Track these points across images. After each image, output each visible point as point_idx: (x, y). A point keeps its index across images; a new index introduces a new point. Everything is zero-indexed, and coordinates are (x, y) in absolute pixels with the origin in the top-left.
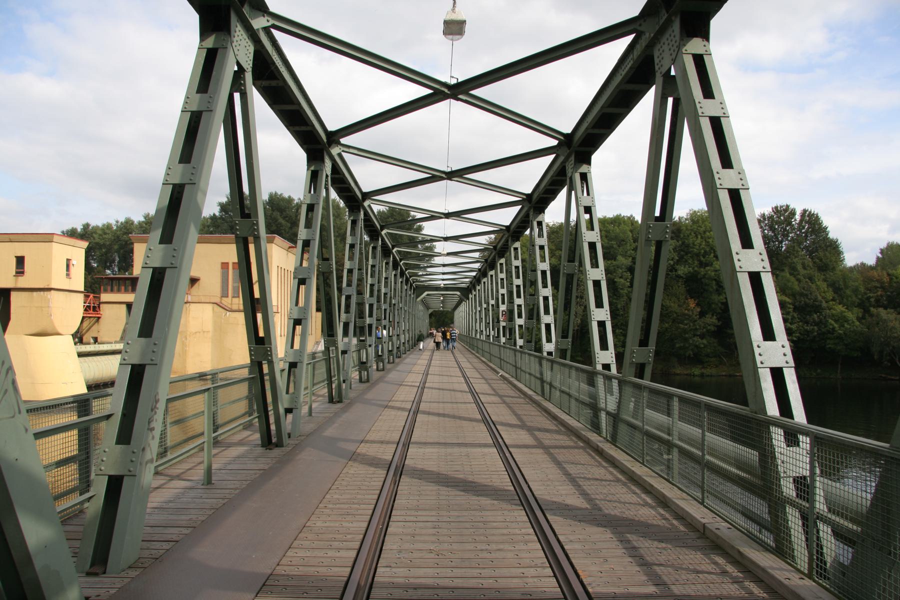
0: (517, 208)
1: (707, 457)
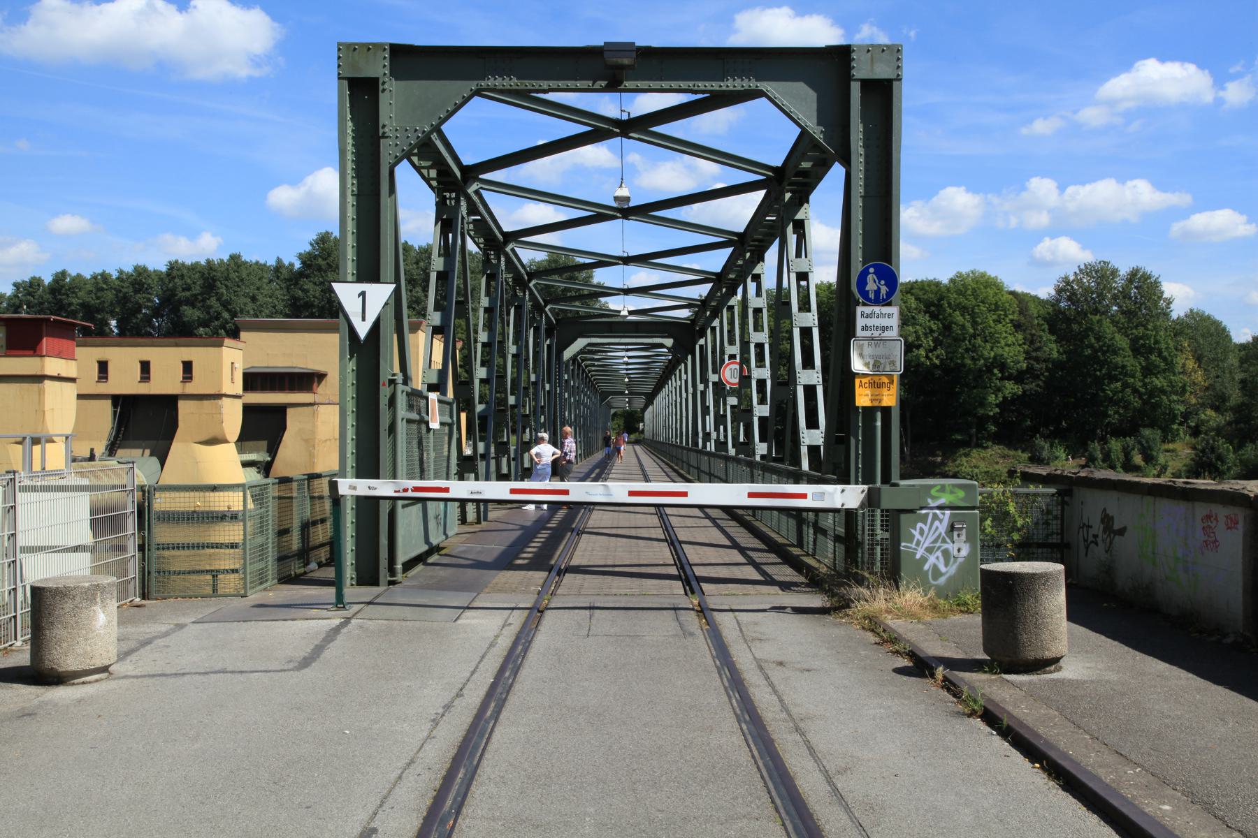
0: (760, 195)
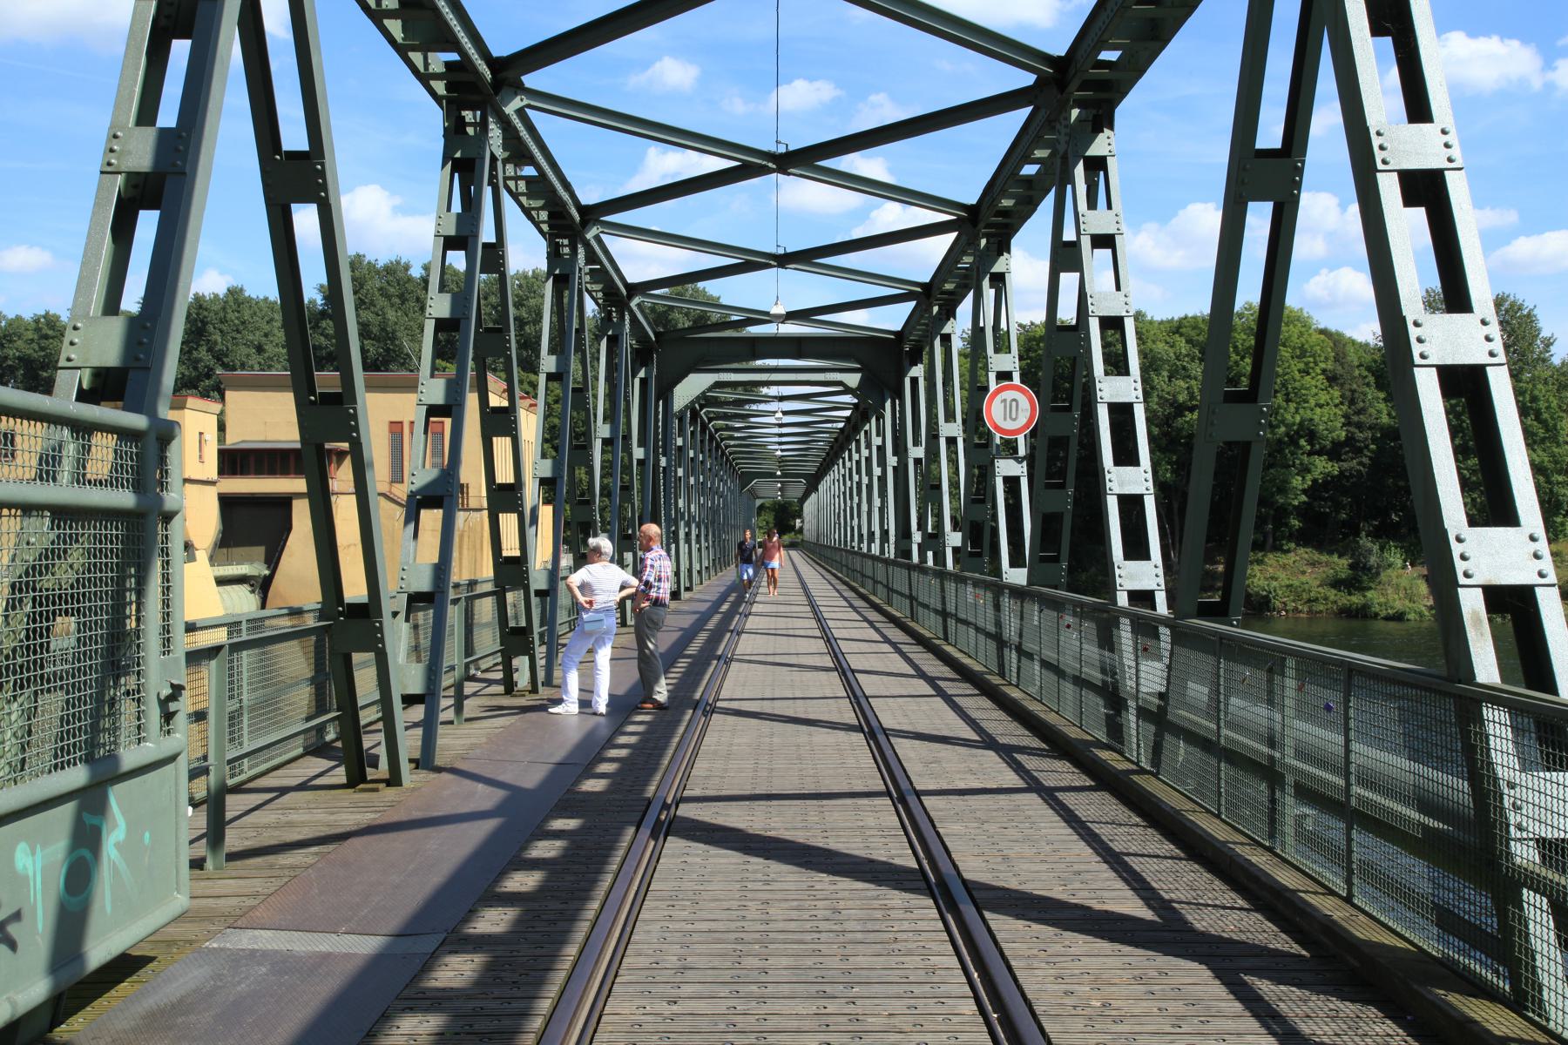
0: (950, 237)
1: (1356, 790)
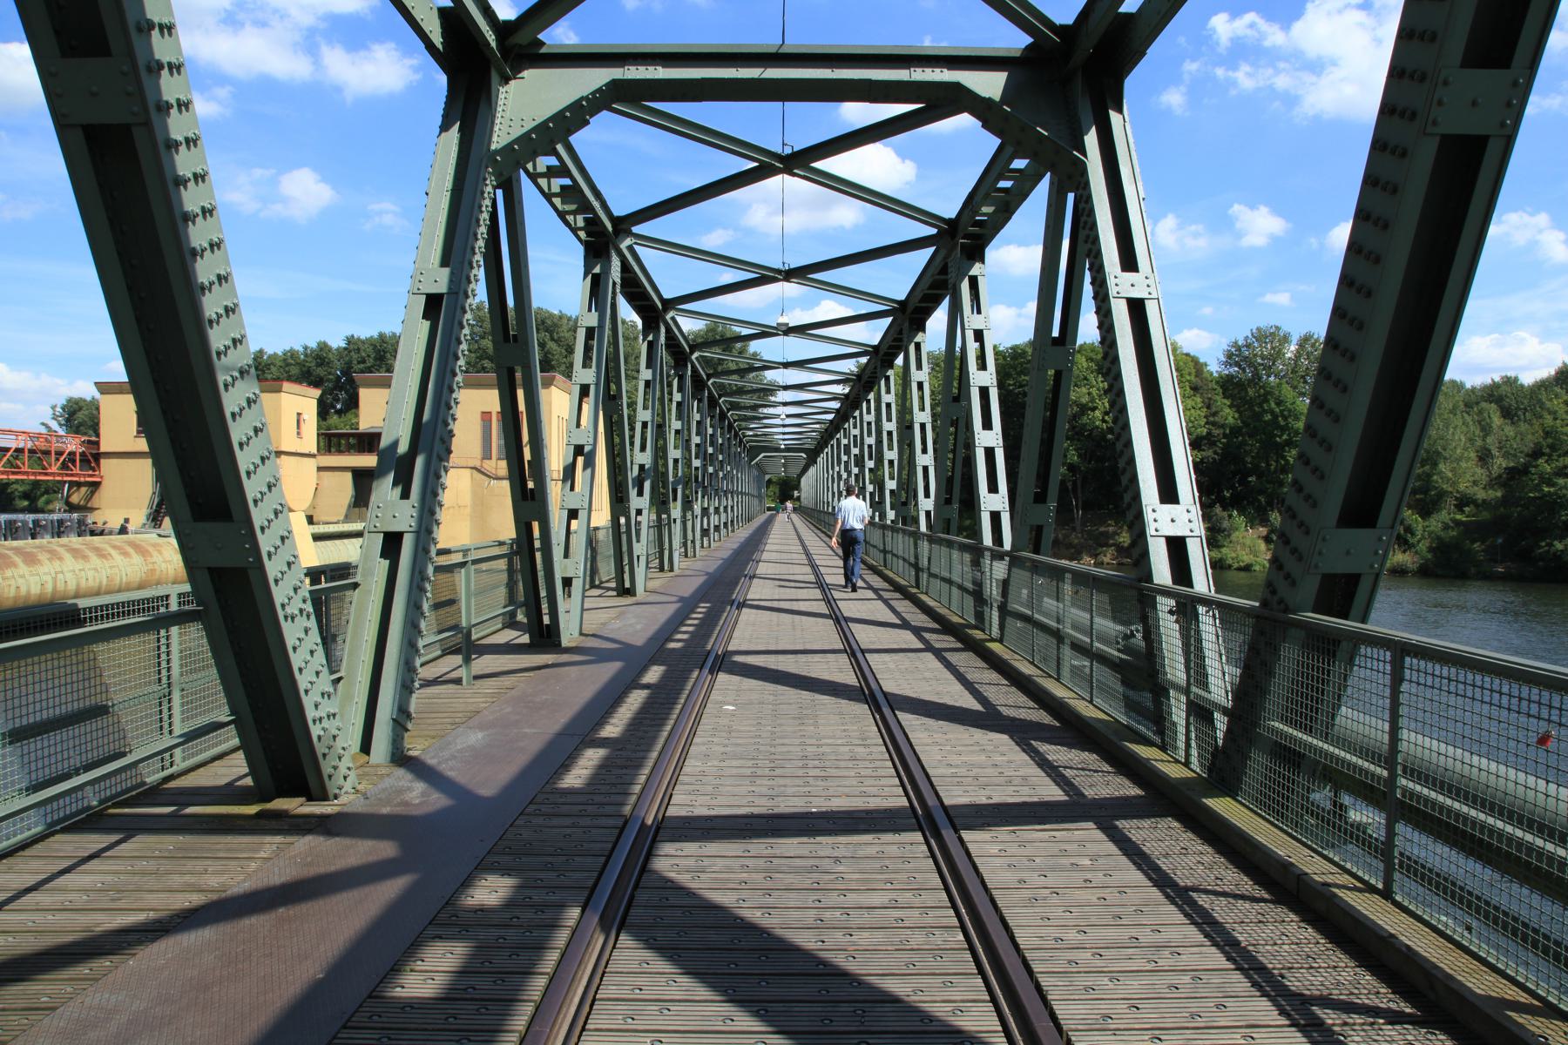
1: (1096, 644)
